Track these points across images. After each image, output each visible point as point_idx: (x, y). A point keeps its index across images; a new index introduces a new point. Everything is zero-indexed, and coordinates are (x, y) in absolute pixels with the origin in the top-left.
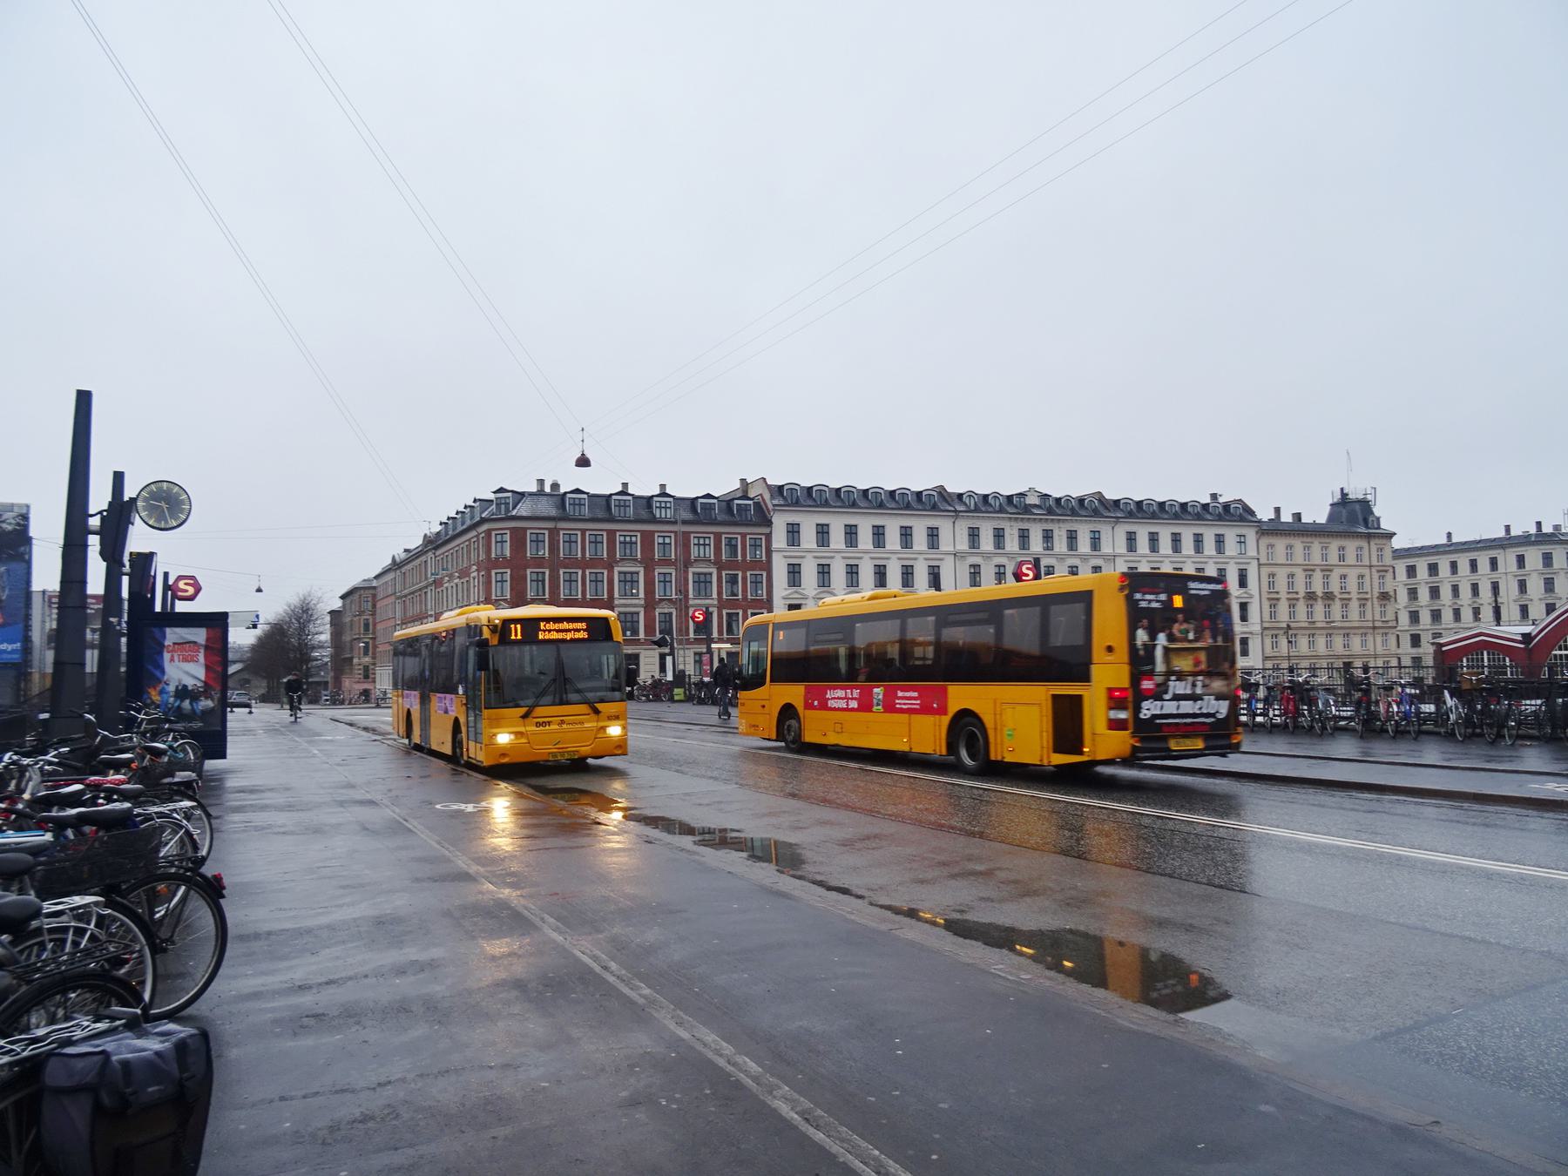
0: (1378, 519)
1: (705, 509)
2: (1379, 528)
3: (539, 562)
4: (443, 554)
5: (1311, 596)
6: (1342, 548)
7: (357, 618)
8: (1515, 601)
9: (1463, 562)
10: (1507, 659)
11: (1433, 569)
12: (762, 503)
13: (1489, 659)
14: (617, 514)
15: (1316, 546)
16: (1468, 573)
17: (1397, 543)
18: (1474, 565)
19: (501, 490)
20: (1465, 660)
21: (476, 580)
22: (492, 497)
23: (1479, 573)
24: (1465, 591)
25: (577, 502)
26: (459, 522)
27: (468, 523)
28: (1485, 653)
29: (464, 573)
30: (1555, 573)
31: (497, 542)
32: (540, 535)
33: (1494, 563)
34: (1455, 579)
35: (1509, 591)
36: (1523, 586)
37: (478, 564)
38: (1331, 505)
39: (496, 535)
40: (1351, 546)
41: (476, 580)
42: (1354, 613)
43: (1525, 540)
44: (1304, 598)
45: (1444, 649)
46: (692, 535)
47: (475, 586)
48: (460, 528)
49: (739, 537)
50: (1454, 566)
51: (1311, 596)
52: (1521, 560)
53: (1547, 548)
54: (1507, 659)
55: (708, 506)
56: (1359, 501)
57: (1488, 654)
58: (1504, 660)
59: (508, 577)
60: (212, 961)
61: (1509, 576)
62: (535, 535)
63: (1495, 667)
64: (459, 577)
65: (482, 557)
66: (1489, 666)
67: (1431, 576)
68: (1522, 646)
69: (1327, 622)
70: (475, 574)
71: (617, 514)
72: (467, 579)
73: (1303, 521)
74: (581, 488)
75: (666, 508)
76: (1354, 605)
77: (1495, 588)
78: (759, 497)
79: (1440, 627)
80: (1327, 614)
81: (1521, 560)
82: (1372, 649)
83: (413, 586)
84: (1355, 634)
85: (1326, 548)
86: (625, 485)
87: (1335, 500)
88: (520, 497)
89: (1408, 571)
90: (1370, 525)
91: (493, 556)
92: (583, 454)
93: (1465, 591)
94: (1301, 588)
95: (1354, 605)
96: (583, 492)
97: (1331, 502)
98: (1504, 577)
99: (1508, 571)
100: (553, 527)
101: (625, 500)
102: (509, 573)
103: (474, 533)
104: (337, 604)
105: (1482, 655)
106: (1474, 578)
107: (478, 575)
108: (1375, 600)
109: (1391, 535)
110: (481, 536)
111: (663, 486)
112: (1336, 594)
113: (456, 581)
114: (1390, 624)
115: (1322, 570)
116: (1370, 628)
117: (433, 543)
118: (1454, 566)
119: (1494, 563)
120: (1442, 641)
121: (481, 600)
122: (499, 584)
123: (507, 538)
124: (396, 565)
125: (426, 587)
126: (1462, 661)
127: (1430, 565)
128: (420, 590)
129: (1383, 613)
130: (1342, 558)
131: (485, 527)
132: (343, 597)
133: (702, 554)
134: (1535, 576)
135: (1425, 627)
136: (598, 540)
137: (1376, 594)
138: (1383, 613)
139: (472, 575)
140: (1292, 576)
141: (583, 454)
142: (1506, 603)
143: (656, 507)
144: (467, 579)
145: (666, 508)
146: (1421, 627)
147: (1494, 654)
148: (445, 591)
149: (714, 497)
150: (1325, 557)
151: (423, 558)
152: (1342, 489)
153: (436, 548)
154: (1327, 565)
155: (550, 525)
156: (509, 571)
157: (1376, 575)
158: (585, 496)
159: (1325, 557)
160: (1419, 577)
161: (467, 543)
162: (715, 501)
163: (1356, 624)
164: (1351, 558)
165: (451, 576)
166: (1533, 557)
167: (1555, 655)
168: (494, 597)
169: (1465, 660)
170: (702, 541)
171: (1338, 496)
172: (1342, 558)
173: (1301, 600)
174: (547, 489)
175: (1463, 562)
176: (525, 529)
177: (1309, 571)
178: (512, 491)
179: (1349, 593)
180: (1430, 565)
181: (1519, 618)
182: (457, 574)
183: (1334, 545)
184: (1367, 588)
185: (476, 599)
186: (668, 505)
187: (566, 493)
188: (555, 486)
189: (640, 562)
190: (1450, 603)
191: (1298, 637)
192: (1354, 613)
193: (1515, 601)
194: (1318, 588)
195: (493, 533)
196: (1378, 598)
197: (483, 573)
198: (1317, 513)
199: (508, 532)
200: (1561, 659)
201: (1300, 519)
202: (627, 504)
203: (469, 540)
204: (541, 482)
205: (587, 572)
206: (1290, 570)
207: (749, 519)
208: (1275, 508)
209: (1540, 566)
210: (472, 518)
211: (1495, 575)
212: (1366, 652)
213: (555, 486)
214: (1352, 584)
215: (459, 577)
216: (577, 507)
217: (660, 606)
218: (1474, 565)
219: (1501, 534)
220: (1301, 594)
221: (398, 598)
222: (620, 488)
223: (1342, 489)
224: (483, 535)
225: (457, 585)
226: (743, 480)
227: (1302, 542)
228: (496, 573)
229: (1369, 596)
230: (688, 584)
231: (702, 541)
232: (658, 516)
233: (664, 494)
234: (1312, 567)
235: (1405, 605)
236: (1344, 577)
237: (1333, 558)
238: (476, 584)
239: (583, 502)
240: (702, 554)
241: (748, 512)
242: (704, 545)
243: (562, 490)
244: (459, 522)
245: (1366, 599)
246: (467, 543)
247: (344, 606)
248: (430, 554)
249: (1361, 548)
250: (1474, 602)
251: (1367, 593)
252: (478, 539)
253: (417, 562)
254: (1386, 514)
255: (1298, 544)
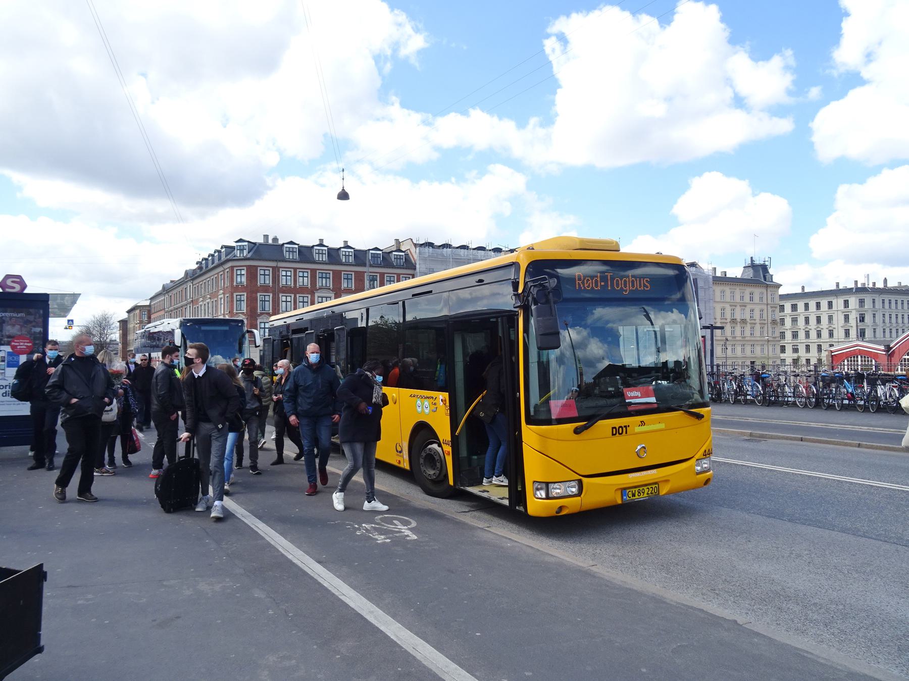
0: (772, 276)
1: (374, 257)
2: (772, 281)
3: (265, 288)
4: (199, 283)
5: (734, 321)
6: (751, 294)
7: (138, 325)
8: (842, 327)
9: (812, 304)
10: (873, 361)
11: (794, 307)
12: (410, 254)
13: (862, 361)
14: (317, 259)
15: (738, 291)
16: (804, 311)
17: (782, 291)
18: (818, 305)
19: (240, 240)
20: (846, 361)
21: (222, 300)
22: (234, 244)
23: (821, 310)
24: (813, 320)
25: (291, 250)
26: (210, 262)
27: (216, 262)
28: (859, 357)
29: (214, 295)
30: (866, 311)
31: (237, 275)
32: (305, 273)
33: (830, 304)
34: (807, 313)
35: (839, 320)
36: (847, 318)
37: (224, 289)
38: (744, 267)
39: (237, 270)
40: (757, 291)
41: (222, 300)
42: (757, 333)
43: (875, 290)
44: (730, 322)
45: (833, 354)
46: (401, 276)
47: (221, 304)
48: (210, 266)
49: (396, 276)
50: (807, 306)
51: (734, 321)
52: (846, 303)
53: (862, 296)
54: (873, 361)
55: (376, 255)
56: (761, 265)
57: (862, 357)
58: (871, 361)
59: (244, 298)
60: (772, 437)
61: (839, 312)
62: (389, 277)
63: (865, 365)
64: (210, 298)
65: (227, 284)
66: (862, 365)
67: (793, 311)
68: (884, 353)
69: (742, 337)
70: (222, 296)
71: (317, 259)
72: (216, 299)
73: (727, 276)
74: (293, 241)
75: (322, 254)
76: (758, 327)
77: (830, 318)
78: (408, 251)
79: (797, 342)
80: (743, 332)
81: (846, 303)
82: (767, 354)
83: (177, 304)
84: (757, 345)
85: (743, 292)
86: (321, 240)
87: (747, 265)
88: (253, 245)
89: (792, 307)
90: (767, 280)
91: (235, 284)
92: (343, 190)
93: (813, 320)
94: (728, 316)
95: (758, 327)
96: (244, 241)
97: (744, 266)
98: (836, 312)
99: (839, 309)
100: (275, 266)
101: (243, 246)
102: (246, 295)
103: (221, 269)
104: (125, 316)
105: (857, 358)
106: (818, 313)
107: (224, 297)
108: (769, 324)
109: (779, 286)
110: (227, 271)
111: (346, 242)
112: (748, 320)
113: (207, 301)
114: (777, 339)
115: (740, 306)
116: (836, 342)
117: (191, 276)
118: (807, 306)
119: (830, 304)
120: (832, 349)
121: (226, 313)
122: (261, 302)
123: (243, 272)
124: (166, 290)
125: (187, 305)
126: (844, 362)
127: (792, 305)
128: (182, 307)
129: (773, 332)
130: (751, 299)
131: (230, 264)
132: (129, 312)
133: (324, 285)
134: (854, 312)
135: (789, 342)
136: (349, 278)
137: (770, 321)
138: (773, 332)
139: (220, 297)
140: (723, 309)
141: (343, 190)
142: (837, 328)
143: (343, 255)
144: (216, 299)
145: (322, 254)
146: (786, 341)
147: (865, 357)
148: (207, 304)
149: (380, 250)
150: (742, 298)
151: (184, 286)
152: (752, 258)
153: (193, 280)
154: (743, 303)
155: (274, 264)
156: (245, 294)
157: (770, 310)
158: (297, 246)
159: (742, 298)
160: (786, 312)
161: (216, 276)
162: (381, 252)
163: (759, 339)
164: (756, 299)
165: (204, 298)
166: (853, 301)
167: (905, 359)
168: (235, 311)
169: (846, 361)
170: (324, 275)
171: (749, 262)
172: (751, 299)
173: (729, 323)
174: (270, 242)
175: (812, 304)
176: (256, 267)
177: (733, 306)
178: (248, 242)
179: (755, 320)
180: (792, 305)
181: (791, 339)
182: (208, 296)
183: (748, 290)
184: (765, 317)
185: (222, 312)
186: (351, 254)
187: (283, 244)
188: (275, 239)
189: (332, 290)
190: (804, 328)
191: (755, 346)
192: (757, 333)
193: (842, 327)
194: (738, 317)
195: (235, 269)
196: (771, 323)
197: (228, 295)
198: (736, 271)
199: (245, 268)
200: (905, 361)
201: (726, 275)
202: (402, 257)
203: (218, 273)
204: (266, 237)
205: (298, 296)
206: (761, 307)
207: (402, 264)
208: (855, 281)
209: (858, 307)
210: (213, 263)
211: (831, 312)
212: (763, 356)
213: (275, 239)
214: (757, 315)
215: (210, 298)
216: (399, 260)
217: (261, 317)
218: (818, 305)
219: (834, 287)
220: (729, 320)
221: (166, 312)
222: (318, 243)
223: (752, 258)
224: (228, 270)
225: (208, 303)
226: (397, 240)
227: (730, 289)
228: (318, 297)
229: (766, 322)
230: (233, 305)
231: (324, 275)
232: (287, 257)
233: (321, 245)
234: (736, 304)
235: (842, 325)
236: (752, 310)
237: (747, 299)
238: (222, 302)
239: (402, 257)
240: (324, 285)
241: (379, 259)
242: (326, 278)
243: (280, 242)
244: (210, 262)
245: (765, 324)
246: (216, 276)
247: (129, 316)
248: (190, 284)
249: (763, 293)
250: (818, 327)
251: (765, 320)
252: (218, 276)
253: (179, 289)
254: (777, 275)
255: (727, 289)
